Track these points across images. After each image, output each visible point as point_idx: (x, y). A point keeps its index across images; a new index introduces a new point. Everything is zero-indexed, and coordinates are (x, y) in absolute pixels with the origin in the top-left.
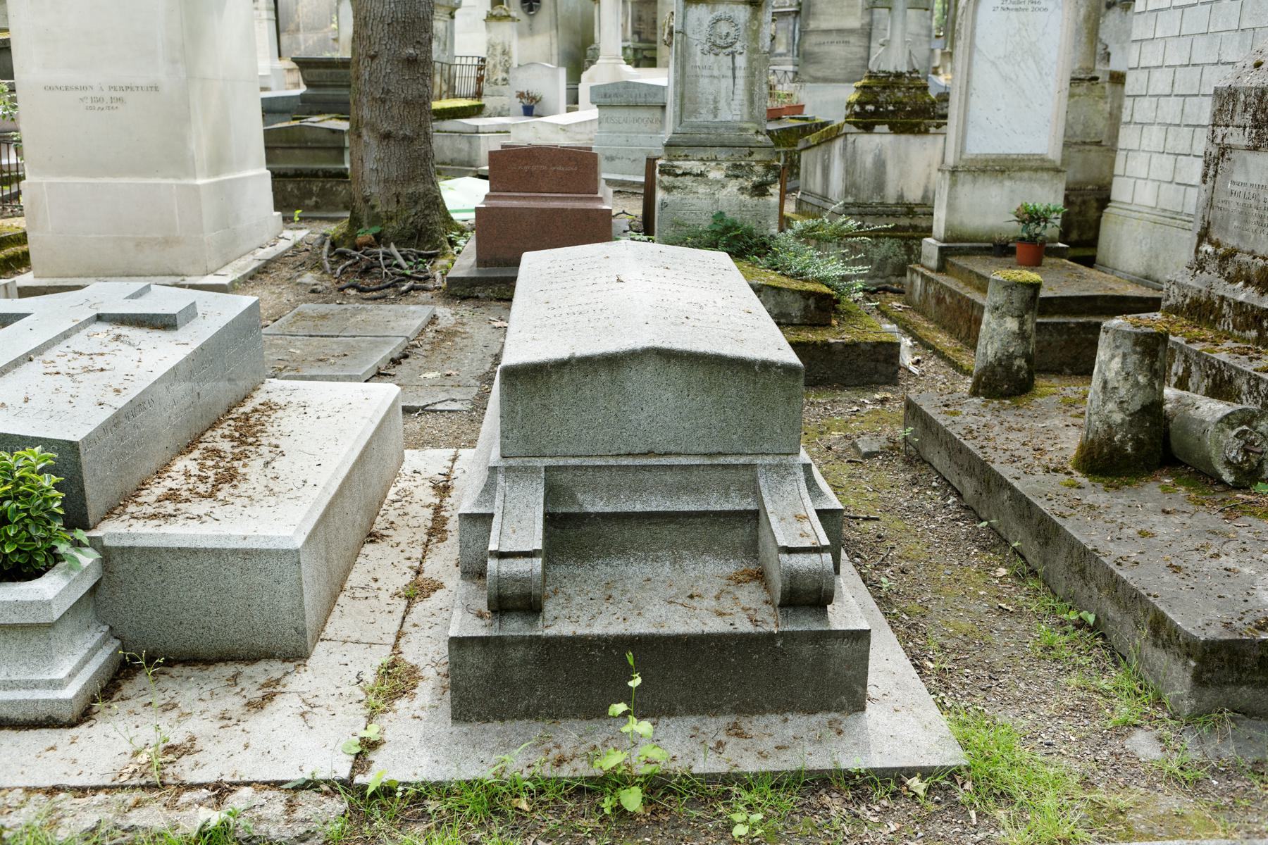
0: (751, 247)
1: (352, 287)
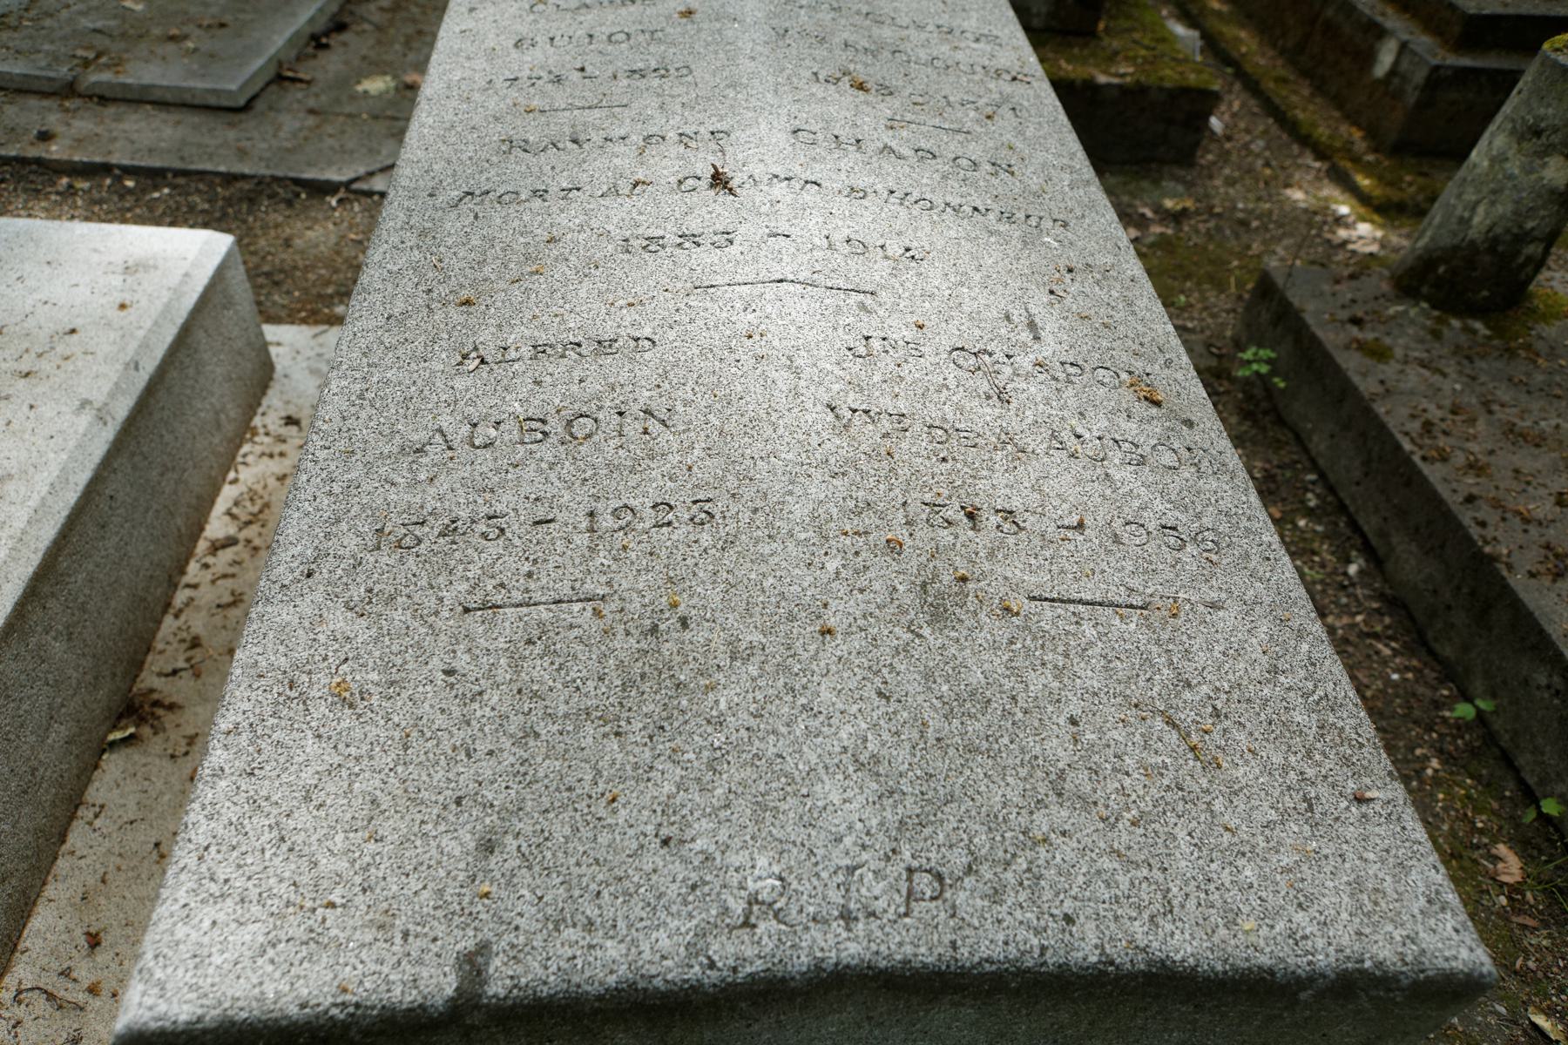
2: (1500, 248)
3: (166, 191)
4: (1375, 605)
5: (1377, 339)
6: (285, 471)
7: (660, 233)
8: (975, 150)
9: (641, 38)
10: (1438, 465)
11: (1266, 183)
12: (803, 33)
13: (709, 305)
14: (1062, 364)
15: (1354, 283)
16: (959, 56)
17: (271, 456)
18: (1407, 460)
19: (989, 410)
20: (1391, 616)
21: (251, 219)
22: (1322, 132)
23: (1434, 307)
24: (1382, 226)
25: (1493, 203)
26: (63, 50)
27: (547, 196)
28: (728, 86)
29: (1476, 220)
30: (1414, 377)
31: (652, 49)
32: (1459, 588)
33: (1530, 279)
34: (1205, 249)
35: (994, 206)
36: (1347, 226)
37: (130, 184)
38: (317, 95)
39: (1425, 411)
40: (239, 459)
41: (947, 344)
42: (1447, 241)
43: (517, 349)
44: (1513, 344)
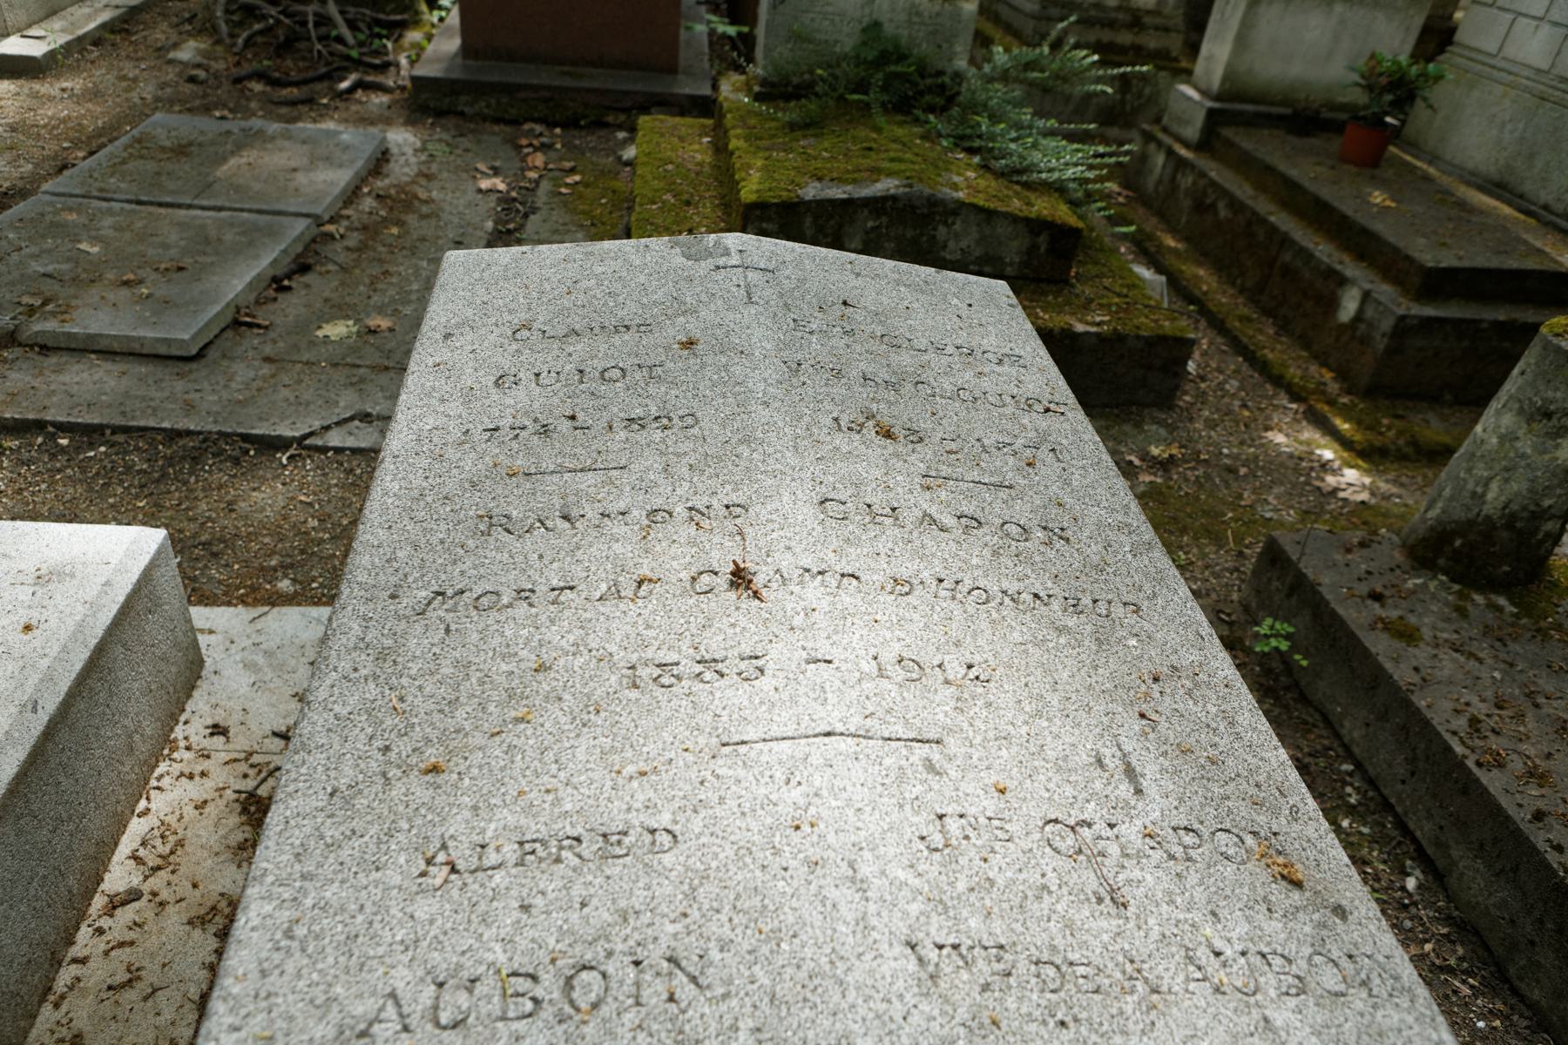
0: (921, 93)
1: (260, 76)
2: (1519, 525)
3: (103, 449)
4: (1444, 931)
5: (1401, 618)
6: (205, 796)
7: (674, 657)
8: (1022, 511)
9: (638, 376)
10: (1495, 771)
11: (1246, 426)
12: (817, 366)
13: (741, 773)
14: (1175, 829)
15: (1365, 552)
16: (986, 383)
17: (191, 777)
18: (1460, 764)
19: (1104, 924)
20: (1462, 944)
21: (193, 479)
22: (1294, 373)
23: (1453, 580)
24: (1367, 472)
25: (1507, 480)
26: (8, 296)
27: (534, 598)
28: (741, 442)
29: (1490, 496)
30: (1448, 665)
31: (651, 389)
32: (1541, 922)
33: (1550, 553)
34: (1197, 498)
35: (1056, 590)
36: (1334, 472)
37: (64, 442)
38: (274, 341)
39: (1467, 704)
40: (153, 783)
41: (1037, 814)
42: (1459, 514)
43: (498, 849)
44: (1543, 624)
